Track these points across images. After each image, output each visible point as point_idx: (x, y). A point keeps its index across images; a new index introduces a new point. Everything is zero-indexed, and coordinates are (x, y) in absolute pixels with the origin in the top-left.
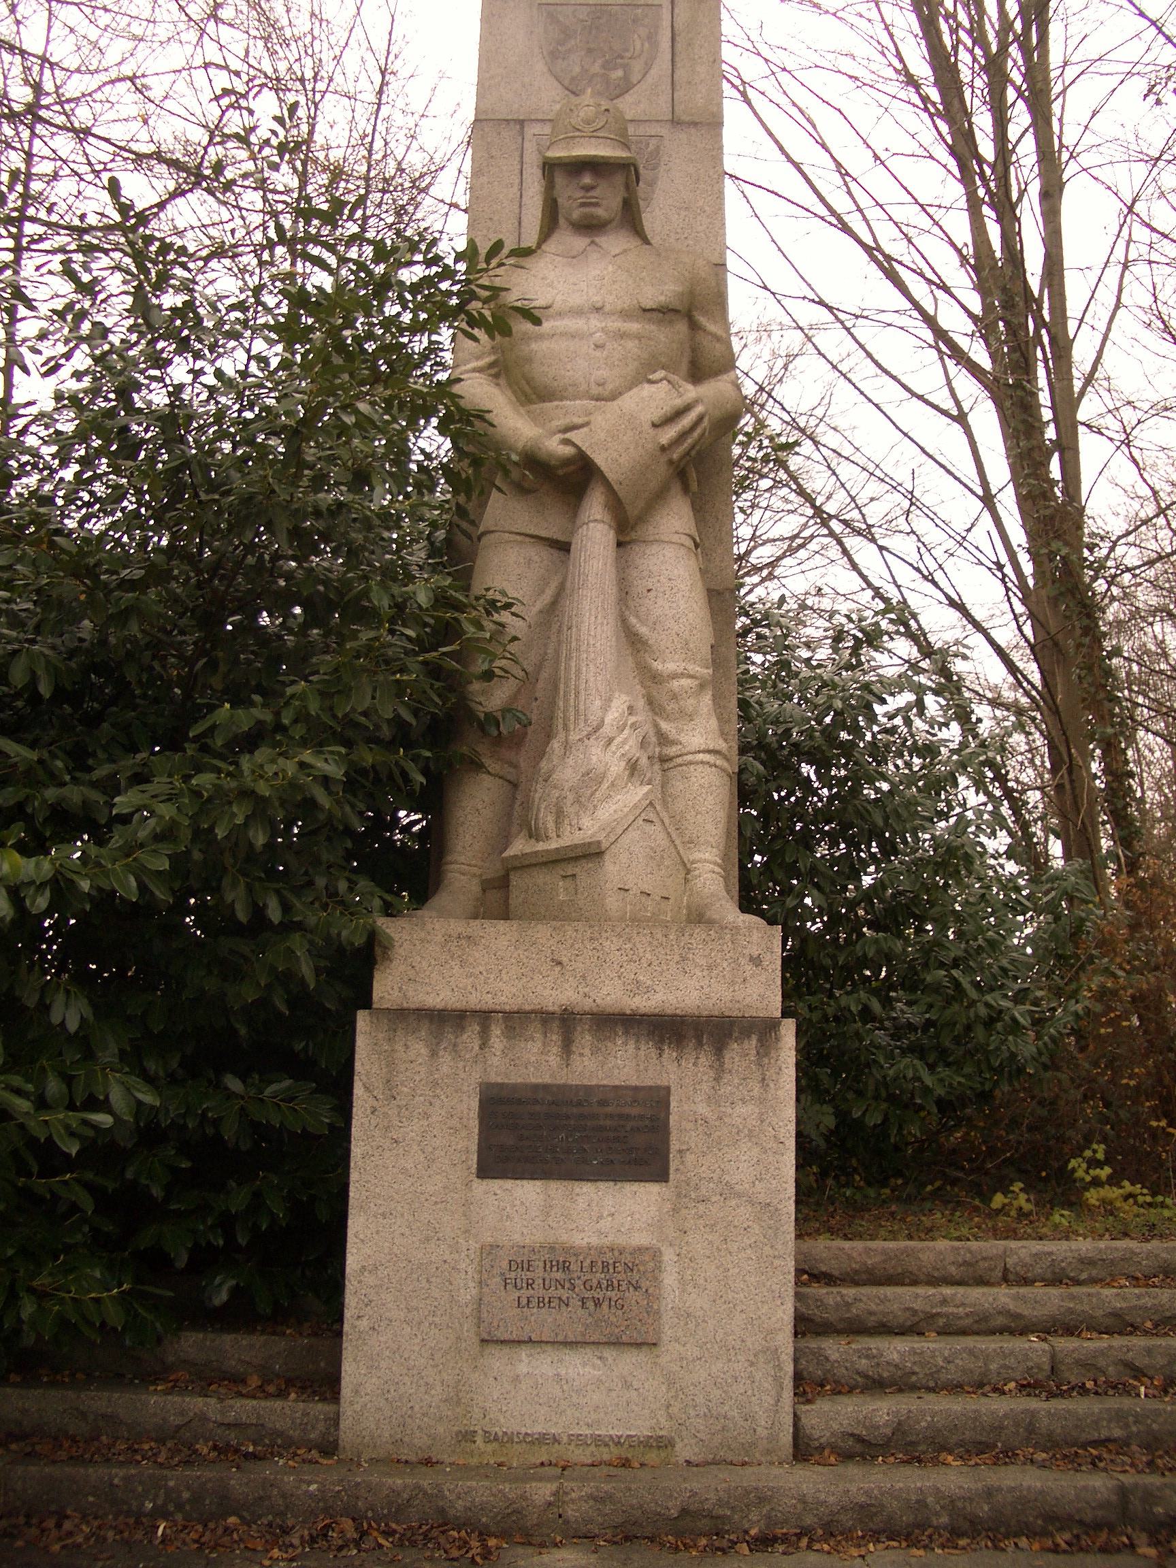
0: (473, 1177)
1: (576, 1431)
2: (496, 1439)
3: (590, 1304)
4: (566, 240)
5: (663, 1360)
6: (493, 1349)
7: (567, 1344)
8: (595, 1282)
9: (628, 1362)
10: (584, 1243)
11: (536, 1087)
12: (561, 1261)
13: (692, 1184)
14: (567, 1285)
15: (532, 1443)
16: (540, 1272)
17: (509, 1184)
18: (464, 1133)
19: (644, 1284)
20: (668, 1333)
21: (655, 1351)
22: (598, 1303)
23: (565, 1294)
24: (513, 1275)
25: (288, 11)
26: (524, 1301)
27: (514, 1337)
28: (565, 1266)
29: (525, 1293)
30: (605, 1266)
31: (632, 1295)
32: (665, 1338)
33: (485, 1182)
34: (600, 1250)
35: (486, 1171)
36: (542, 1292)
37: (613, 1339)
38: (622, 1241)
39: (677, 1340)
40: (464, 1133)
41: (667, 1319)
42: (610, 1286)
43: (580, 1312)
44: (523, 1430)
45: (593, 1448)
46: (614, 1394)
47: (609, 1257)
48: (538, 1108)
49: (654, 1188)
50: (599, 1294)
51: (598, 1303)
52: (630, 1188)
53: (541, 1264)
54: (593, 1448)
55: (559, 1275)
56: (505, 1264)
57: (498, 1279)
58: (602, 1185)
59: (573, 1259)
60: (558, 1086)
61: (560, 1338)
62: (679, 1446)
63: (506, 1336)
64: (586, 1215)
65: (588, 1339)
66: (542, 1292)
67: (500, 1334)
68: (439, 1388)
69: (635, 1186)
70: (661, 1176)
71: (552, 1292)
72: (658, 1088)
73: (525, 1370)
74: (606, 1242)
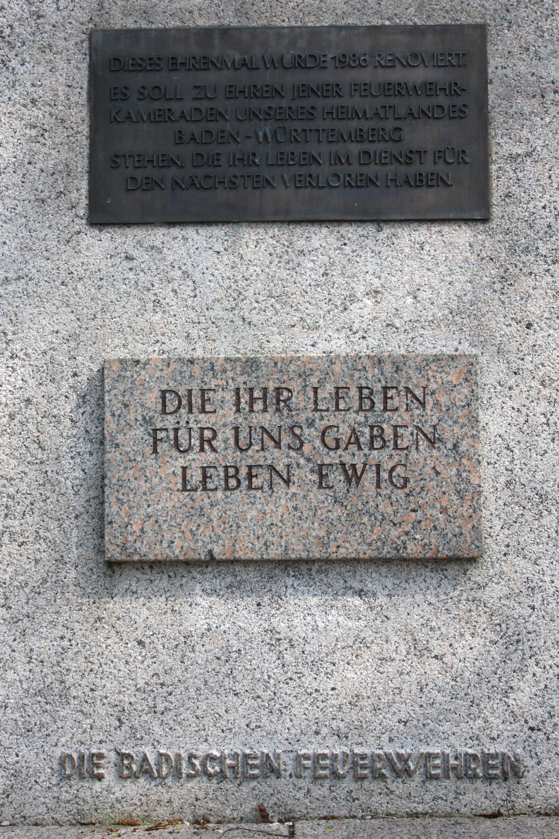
0: (81, 224)
1: (310, 749)
2: (145, 771)
3: (336, 478)
4: (443, 150)
5: (494, 592)
6: (127, 580)
7: (289, 565)
8: (345, 431)
9: (415, 607)
10: (316, 353)
11: (206, 33)
12: (268, 389)
13: (540, 224)
14: (286, 439)
15: (221, 776)
16: (227, 414)
17: (158, 235)
18: (61, 136)
19: (449, 432)
20: (496, 535)
21: (477, 574)
22: (353, 476)
23: (280, 458)
24: (170, 421)
25: (249, 830)
26: (196, 477)
27: (177, 552)
28: (279, 399)
29: (197, 460)
30: (365, 395)
31: (423, 455)
32: (493, 548)
33: (106, 235)
34: (354, 363)
35: (103, 214)
36: (232, 456)
37: (387, 551)
38: (396, 346)
39: (521, 552)
40: (61, 136)
41: (492, 503)
42: (377, 438)
43: (317, 496)
44: (202, 750)
45: (348, 784)
46: (390, 669)
47: (372, 378)
48: (211, 77)
49: (461, 235)
50: (355, 458)
51: (353, 476)
52: (408, 237)
53: (229, 397)
54: (348, 784)
55: (269, 419)
56: (152, 399)
57: (139, 432)
58: (350, 232)
59: (296, 385)
60: (253, 31)
61: (274, 553)
62: (530, 778)
63: (160, 552)
64: (320, 294)
65: (332, 552)
66: (232, 456)
67: (149, 549)
68: (22, 668)
69: (421, 233)
70: (475, 209)
71: (254, 455)
72: (459, 30)
73: (202, 625)
74: (363, 348)
